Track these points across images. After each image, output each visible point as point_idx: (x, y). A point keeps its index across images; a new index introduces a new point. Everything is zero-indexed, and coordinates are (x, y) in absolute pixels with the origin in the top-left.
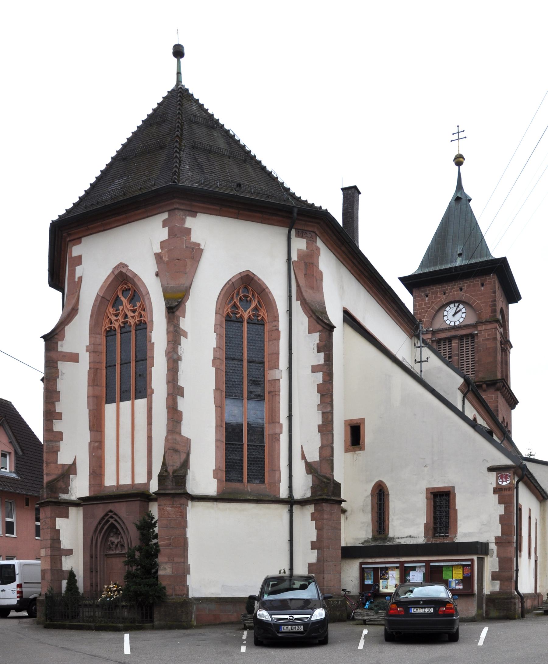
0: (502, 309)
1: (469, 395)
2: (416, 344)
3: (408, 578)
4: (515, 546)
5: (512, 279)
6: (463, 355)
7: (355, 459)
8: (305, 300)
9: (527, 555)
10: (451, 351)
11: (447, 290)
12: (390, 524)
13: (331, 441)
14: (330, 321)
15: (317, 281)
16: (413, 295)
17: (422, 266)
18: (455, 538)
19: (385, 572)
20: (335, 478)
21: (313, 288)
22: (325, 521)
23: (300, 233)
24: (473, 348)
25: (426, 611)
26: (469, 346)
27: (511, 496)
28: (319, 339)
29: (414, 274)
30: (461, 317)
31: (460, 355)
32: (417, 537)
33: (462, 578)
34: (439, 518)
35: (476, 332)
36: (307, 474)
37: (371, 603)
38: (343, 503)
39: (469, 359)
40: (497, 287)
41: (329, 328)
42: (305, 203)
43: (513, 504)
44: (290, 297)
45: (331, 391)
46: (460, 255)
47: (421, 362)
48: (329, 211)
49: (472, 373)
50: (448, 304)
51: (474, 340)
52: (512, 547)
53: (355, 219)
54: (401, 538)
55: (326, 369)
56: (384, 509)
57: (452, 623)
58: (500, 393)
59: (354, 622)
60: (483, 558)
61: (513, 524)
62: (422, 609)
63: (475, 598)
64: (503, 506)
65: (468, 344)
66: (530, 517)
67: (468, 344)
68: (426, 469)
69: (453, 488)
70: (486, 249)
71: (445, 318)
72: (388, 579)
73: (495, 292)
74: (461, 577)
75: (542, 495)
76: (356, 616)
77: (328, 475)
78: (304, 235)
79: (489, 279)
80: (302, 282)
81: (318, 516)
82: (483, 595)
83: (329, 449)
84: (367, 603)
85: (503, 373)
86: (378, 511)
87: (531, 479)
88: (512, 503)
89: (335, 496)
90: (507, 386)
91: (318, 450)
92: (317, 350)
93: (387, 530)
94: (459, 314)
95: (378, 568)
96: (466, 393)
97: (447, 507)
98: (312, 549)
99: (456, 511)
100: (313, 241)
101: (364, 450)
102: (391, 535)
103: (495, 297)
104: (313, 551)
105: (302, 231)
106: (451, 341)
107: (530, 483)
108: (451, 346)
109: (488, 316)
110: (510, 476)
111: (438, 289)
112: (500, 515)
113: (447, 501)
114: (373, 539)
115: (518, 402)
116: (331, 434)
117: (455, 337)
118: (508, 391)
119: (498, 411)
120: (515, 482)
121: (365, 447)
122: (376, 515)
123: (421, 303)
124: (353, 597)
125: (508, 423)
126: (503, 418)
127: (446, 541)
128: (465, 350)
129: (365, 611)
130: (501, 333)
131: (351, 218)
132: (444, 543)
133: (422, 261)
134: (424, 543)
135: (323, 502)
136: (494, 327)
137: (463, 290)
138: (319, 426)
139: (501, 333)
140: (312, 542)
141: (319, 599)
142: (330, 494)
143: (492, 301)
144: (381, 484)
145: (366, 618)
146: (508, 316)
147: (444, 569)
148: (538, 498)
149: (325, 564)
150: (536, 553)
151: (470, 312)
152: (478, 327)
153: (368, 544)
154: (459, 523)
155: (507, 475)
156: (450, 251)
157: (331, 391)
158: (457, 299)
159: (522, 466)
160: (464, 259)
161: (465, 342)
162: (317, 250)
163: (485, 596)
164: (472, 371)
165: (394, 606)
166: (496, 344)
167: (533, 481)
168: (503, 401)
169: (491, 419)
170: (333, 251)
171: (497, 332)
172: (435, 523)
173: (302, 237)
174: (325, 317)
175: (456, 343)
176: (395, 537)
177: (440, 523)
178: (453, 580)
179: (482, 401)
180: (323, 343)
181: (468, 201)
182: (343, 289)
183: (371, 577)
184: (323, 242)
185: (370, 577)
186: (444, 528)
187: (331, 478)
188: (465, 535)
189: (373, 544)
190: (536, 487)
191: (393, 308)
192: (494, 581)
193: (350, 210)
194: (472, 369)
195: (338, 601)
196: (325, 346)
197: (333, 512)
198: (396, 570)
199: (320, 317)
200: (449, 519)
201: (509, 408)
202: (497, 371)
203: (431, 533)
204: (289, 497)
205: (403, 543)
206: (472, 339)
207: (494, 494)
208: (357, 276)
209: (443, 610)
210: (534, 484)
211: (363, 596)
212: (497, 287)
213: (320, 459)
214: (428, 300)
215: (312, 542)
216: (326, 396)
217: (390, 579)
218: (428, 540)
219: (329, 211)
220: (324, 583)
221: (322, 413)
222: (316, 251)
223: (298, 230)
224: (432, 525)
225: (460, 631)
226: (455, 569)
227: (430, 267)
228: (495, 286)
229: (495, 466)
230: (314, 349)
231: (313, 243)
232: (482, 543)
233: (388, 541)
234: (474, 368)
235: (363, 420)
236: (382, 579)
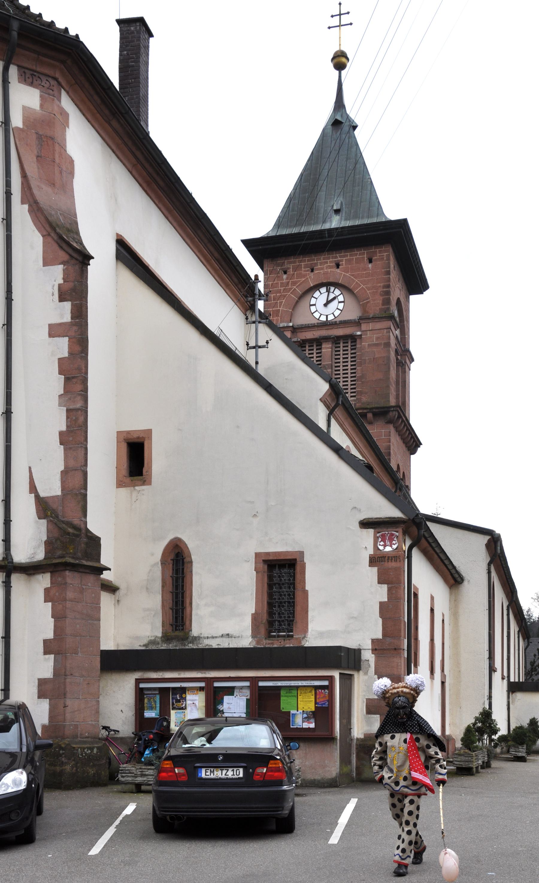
0: (398, 302)
1: (338, 412)
2: (249, 318)
3: (220, 707)
4: (406, 657)
5: (415, 256)
6: (339, 366)
7: (134, 498)
8: (36, 202)
9: (428, 672)
10: (320, 360)
11: (316, 264)
12: (194, 612)
13: (83, 461)
14: (84, 247)
15: (61, 173)
16: (265, 269)
17: (279, 224)
18: (304, 640)
19: (181, 697)
20: (89, 527)
21: (54, 184)
22: (68, 604)
23: (27, 77)
24: (355, 357)
25: (230, 774)
26: (347, 354)
27: (399, 570)
28: (62, 276)
29: (266, 236)
30: (337, 309)
31: (334, 367)
32: (239, 637)
33: (313, 709)
34: (277, 605)
35: (359, 333)
36: (39, 518)
37: (153, 751)
38: (104, 572)
39: (347, 373)
40: (392, 266)
41: (80, 258)
42: (38, 18)
43: (402, 585)
44: (8, 194)
45: (83, 371)
46: (337, 212)
47: (257, 347)
48: (81, 39)
49: (352, 395)
50: (317, 287)
51: (355, 345)
52: (401, 657)
53: (142, 81)
54: (213, 637)
55: (75, 332)
56: (183, 586)
57: (282, 796)
58: (394, 427)
59: (119, 787)
60: (351, 675)
61: (402, 618)
62: (222, 770)
63: (336, 745)
64: (385, 587)
65: (347, 350)
66: (432, 610)
67: (347, 350)
68: (255, 521)
69: (302, 553)
70: (377, 205)
71: (313, 309)
72: (185, 708)
73: (388, 273)
74: (311, 707)
75: (452, 575)
76: (123, 777)
77: (76, 521)
78: (35, 81)
79: (380, 252)
80: (32, 170)
81: (57, 594)
82: (352, 740)
83: (79, 476)
84: (147, 752)
85: (399, 399)
86: (173, 590)
87: (434, 545)
88: (399, 582)
89: (92, 560)
90: (403, 417)
91: (58, 477)
92: (59, 297)
93: (187, 623)
94: (334, 304)
95: (168, 689)
96: (333, 408)
97: (292, 586)
98: (46, 652)
99: (305, 593)
100: (53, 96)
101: (150, 483)
102: (195, 631)
103: (389, 280)
104: (47, 656)
105: (32, 72)
106: (321, 345)
107: (433, 552)
108: (320, 353)
109: (378, 308)
110: (397, 537)
111: (304, 262)
112: (60, 359)
113: (291, 576)
114: (163, 639)
115: (421, 444)
116: (83, 449)
117: (326, 339)
118: (405, 425)
119: (389, 454)
120: (405, 548)
121: (153, 480)
122: (169, 597)
123: (276, 283)
124: (122, 740)
125: (405, 474)
126: (398, 465)
127: (289, 644)
128: (341, 360)
129: (138, 767)
130: (397, 337)
131: (135, 79)
132: (284, 648)
133: (279, 217)
134: (252, 647)
135: (66, 570)
136: (386, 327)
137: (340, 267)
138: (61, 434)
139: (397, 338)
140: (45, 641)
141: (21, 749)
142: (79, 554)
143: (384, 287)
144: (178, 543)
145: (139, 779)
146: (409, 313)
147: (283, 693)
148: (446, 580)
149: (68, 680)
150: (443, 670)
151: (351, 301)
152: (362, 324)
153: (154, 647)
154: (310, 614)
155: (392, 535)
156: (322, 204)
157: (83, 371)
158: (331, 280)
159: (417, 521)
160: (343, 218)
161: (341, 347)
162: (61, 114)
163: (355, 741)
164: (351, 393)
165: (167, 764)
166: (389, 352)
167: (436, 549)
168: (397, 441)
169: (369, 448)
170: (96, 126)
171: (391, 334)
172: (270, 614)
173: (31, 84)
174: (74, 239)
175: (328, 348)
176: (202, 636)
177: (279, 614)
178: (298, 712)
179: (359, 424)
180: (71, 285)
181: (351, 129)
182: (116, 200)
183: (156, 705)
184: (76, 105)
185: (154, 706)
186: (286, 623)
187: (83, 526)
188: (321, 635)
189: (164, 647)
190: (442, 561)
191: (212, 254)
192: (370, 716)
193: (132, 62)
194: (351, 389)
195: (92, 749)
196: (74, 290)
197: (84, 587)
198: (199, 692)
199: (65, 238)
200: (294, 606)
201: (408, 453)
202: (389, 393)
203: (263, 630)
204: (3, 558)
205: (215, 646)
206: (353, 344)
207: (369, 566)
208: (144, 185)
209: (262, 773)
210: (440, 554)
211: (140, 739)
212: (392, 266)
213: (62, 492)
214: (287, 278)
215: (45, 641)
216: (74, 380)
217: (189, 709)
218: (258, 643)
219: (82, 39)
220: (65, 715)
221: (68, 411)
222: (58, 116)
223: (23, 70)
224: (265, 616)
225: (297, 812)
226: (301, 693)
227: (290, 227)
228: (389, 263)
229: (372, 518)
230: (53, 295)
231: (53, 100)
232: (348, 650)
233: (190, 643)
234: (355, 388)
235: (149, 432)
236: (174, 708)
